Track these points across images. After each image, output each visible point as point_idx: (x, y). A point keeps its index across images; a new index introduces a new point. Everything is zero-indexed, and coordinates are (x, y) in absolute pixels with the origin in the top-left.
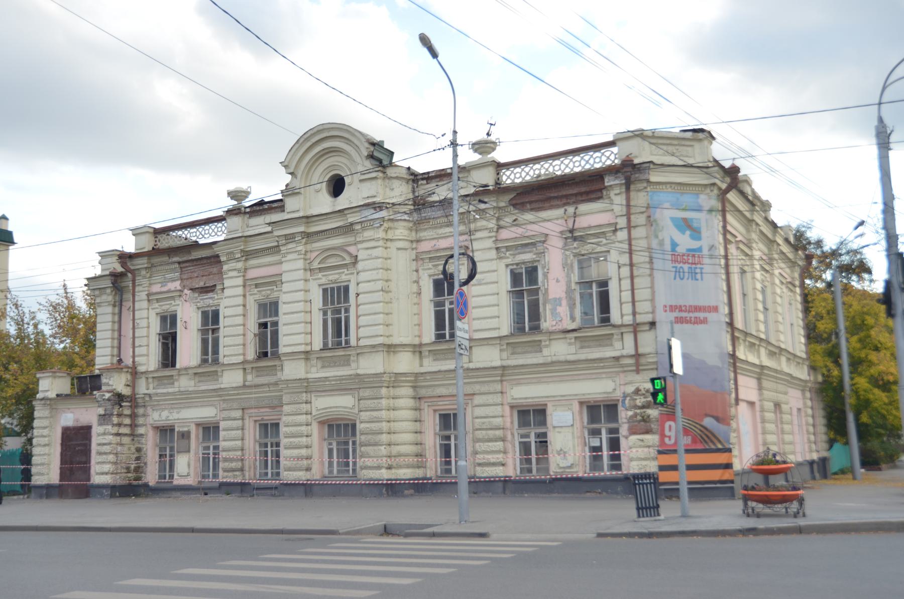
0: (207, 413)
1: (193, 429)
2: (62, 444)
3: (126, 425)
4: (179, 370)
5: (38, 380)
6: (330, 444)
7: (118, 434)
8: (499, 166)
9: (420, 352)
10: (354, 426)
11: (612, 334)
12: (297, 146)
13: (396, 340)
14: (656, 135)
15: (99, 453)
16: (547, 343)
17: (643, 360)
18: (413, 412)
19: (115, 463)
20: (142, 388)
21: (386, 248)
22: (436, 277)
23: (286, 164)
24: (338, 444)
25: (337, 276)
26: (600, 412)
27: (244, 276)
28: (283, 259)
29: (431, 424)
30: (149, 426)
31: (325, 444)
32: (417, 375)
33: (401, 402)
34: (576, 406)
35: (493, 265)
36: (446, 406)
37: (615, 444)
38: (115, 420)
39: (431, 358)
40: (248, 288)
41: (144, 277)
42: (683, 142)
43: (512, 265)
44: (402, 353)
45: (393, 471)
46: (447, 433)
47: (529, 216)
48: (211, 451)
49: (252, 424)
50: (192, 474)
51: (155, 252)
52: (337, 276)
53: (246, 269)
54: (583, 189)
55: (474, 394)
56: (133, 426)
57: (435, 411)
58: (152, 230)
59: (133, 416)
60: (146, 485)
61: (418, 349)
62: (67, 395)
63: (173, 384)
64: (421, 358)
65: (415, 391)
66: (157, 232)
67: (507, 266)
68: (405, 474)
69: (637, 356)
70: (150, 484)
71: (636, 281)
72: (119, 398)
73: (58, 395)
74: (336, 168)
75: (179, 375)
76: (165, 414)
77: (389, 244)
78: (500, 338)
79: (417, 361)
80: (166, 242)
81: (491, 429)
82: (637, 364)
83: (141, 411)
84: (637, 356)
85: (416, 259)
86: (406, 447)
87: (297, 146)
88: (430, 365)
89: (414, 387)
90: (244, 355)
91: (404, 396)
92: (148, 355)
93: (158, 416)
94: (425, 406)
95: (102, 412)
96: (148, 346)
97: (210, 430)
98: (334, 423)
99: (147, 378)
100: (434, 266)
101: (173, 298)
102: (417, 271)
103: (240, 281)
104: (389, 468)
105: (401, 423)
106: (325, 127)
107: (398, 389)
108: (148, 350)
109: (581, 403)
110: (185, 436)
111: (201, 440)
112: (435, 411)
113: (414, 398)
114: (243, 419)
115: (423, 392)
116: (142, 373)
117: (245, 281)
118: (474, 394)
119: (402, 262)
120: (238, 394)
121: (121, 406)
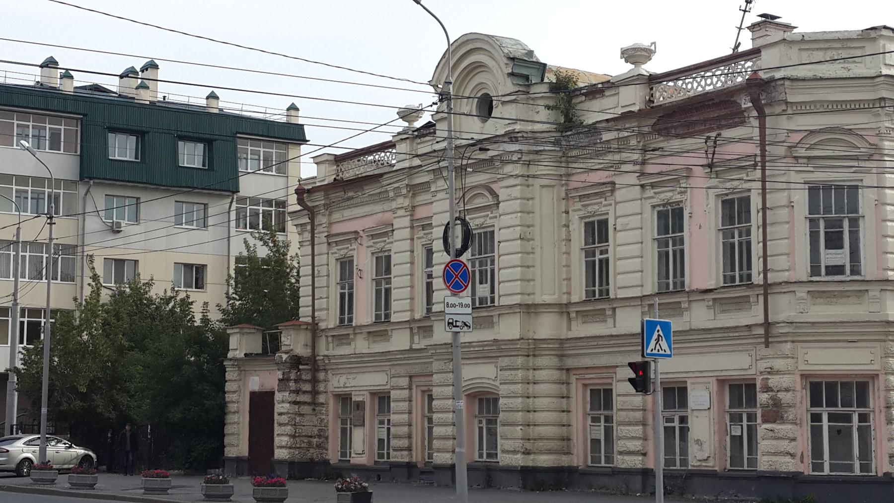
0: (376, 380)
1: (367, 399)
2: (250, 412)
3: (305, 392)
4: (355, 328)
5: (229, 335)
6: (480, 422)
7: (295, 403)
8: (653, 80)
9: (568, 313)
10: (496, 400)
11: (748, 296)
12: (444, 60)
13: (539, 299)
14: (806, 38)
15: (280, 425)
16: (686, 305)
17: (775, 331)
18: (558, 386)
19: (293, 436)
20: (324, 349)
21: (528, 186)
22: (587, 220)
23: (433, 83)
24: (832, 417)
25: (482, 220)
26: (740, 392)
27: (412, 215)
28: (434, 199)
29: (579, 401)
30: (330, 395)
31: (476, 421)
32: (562, 341)
33: (542, 375)
34: (714, 386)
35: (635, 207)
36: (596, 380)
37: (752, 431)
38: (292, 385)
39: (580, 321)
40: (416, 230)
41: (324, 215)
42: (845, 44)
43: (659, 205)
44: (546, 314)
45: (532, 457)
46: (816, 410)
47: (675, 144)
48: (676, 424)
49: (580, 388)
50: (366, 451)
51: (339, 184)
52: (482, 220)
53: (414, 208)
54: (723, 112)
55: (617, 366)
56: (315, 393)
57: (585, 385)
58: (332, 158)
59: (314, 381)
60: (326, 462)
61: (563, 309)
62: (257, 354)
63: (350, 344)
64: (570, 320)
65: (561, 360)
66: (338, 160)
67: (654, 207)
68: (544, 460)
69: (767, 324)
70: (331, 462)
71: (768, 229)
72: (296, 361)
73: (246, 355)
74: (484, 86)
75: (355, 334)
76: (343, 379)
77: (531, 181)
78: (642, 298)
79: (565, 324)
80: (351, 171)
81: (632, 410)
82: (767, 335)
83: (321, 376)
84: (767, 324)
85: (567, 198)
86: (547, 428)
87: (444, 60)
88: (581, 329)
89: (561, 357)
90: (412, 310)
91: (547, 370)
92: (328, 310)
93: (337, 382)
94: (573, 379)
95: (281, 377)
96: (328, 298)
97: (383, 399)
98: (484, 397)
99: (327, 337)
100: (584, 206)
101: (348, 241)
102: (567, 212)
103: (406, 221)
104: (527, 453)
105: (541, 400)
106: (469, 37)
107: (539, 359)
108: (328, 302)
109: (721, 382)
110: (360, 406)
111: (376, 412)
112: (585, 385)
113: (560, 369)
114: (410, 388)
115: (570, 363)
116: (323, 330)
117: (567, 191)
118: (617, 366)
119: (547, 201)
120: (405, 359)
121: (299, 370)
